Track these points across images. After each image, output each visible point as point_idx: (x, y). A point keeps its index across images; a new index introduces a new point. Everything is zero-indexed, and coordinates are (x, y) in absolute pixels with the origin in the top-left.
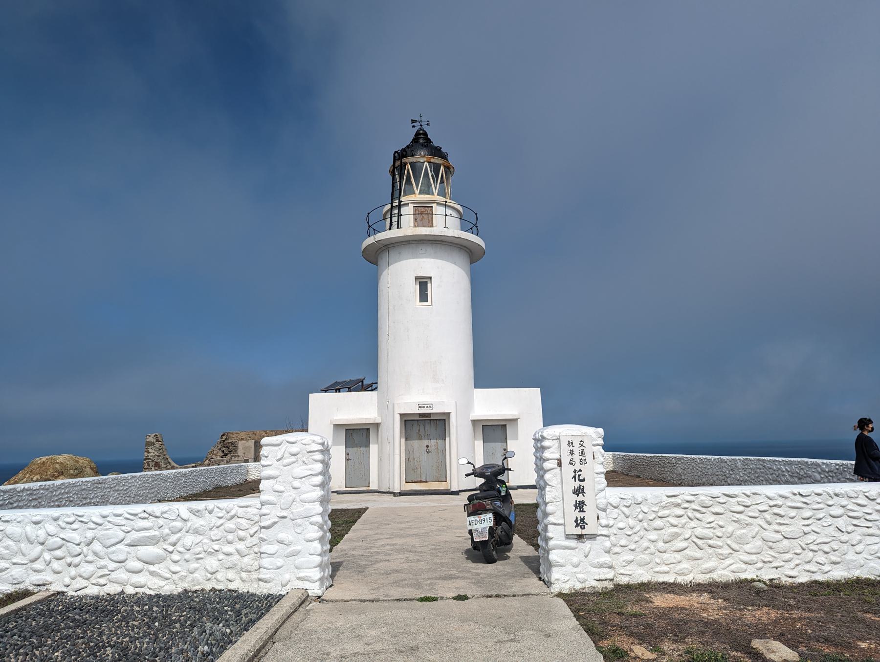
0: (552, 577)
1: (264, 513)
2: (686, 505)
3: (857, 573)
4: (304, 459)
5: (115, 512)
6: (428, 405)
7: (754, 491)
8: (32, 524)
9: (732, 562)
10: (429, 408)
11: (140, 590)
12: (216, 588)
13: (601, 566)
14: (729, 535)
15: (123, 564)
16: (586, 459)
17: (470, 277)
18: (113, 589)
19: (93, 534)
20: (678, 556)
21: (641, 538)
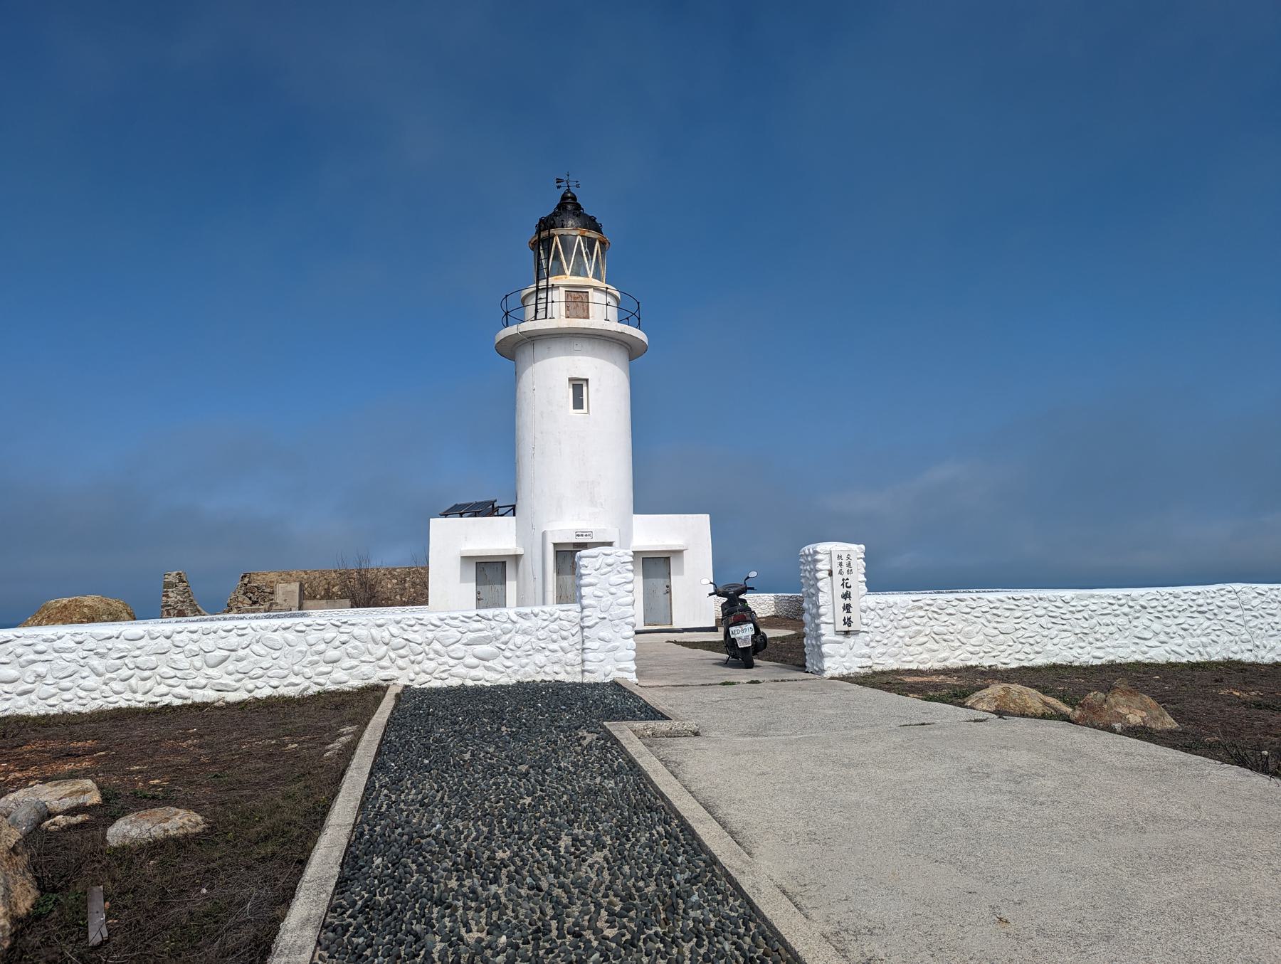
2: (927, 608)
3: (1054, 660)
4: (618, 569)
5: (452, 616)
7: (978, 596)
8: (376, 627)
9: (961, 652)
10: (588, 537)
13: (863, 656)
14: (959, 631)
15: (461, 661)
17: (628, 375)
18: (455, 682)
20: (920, 649)
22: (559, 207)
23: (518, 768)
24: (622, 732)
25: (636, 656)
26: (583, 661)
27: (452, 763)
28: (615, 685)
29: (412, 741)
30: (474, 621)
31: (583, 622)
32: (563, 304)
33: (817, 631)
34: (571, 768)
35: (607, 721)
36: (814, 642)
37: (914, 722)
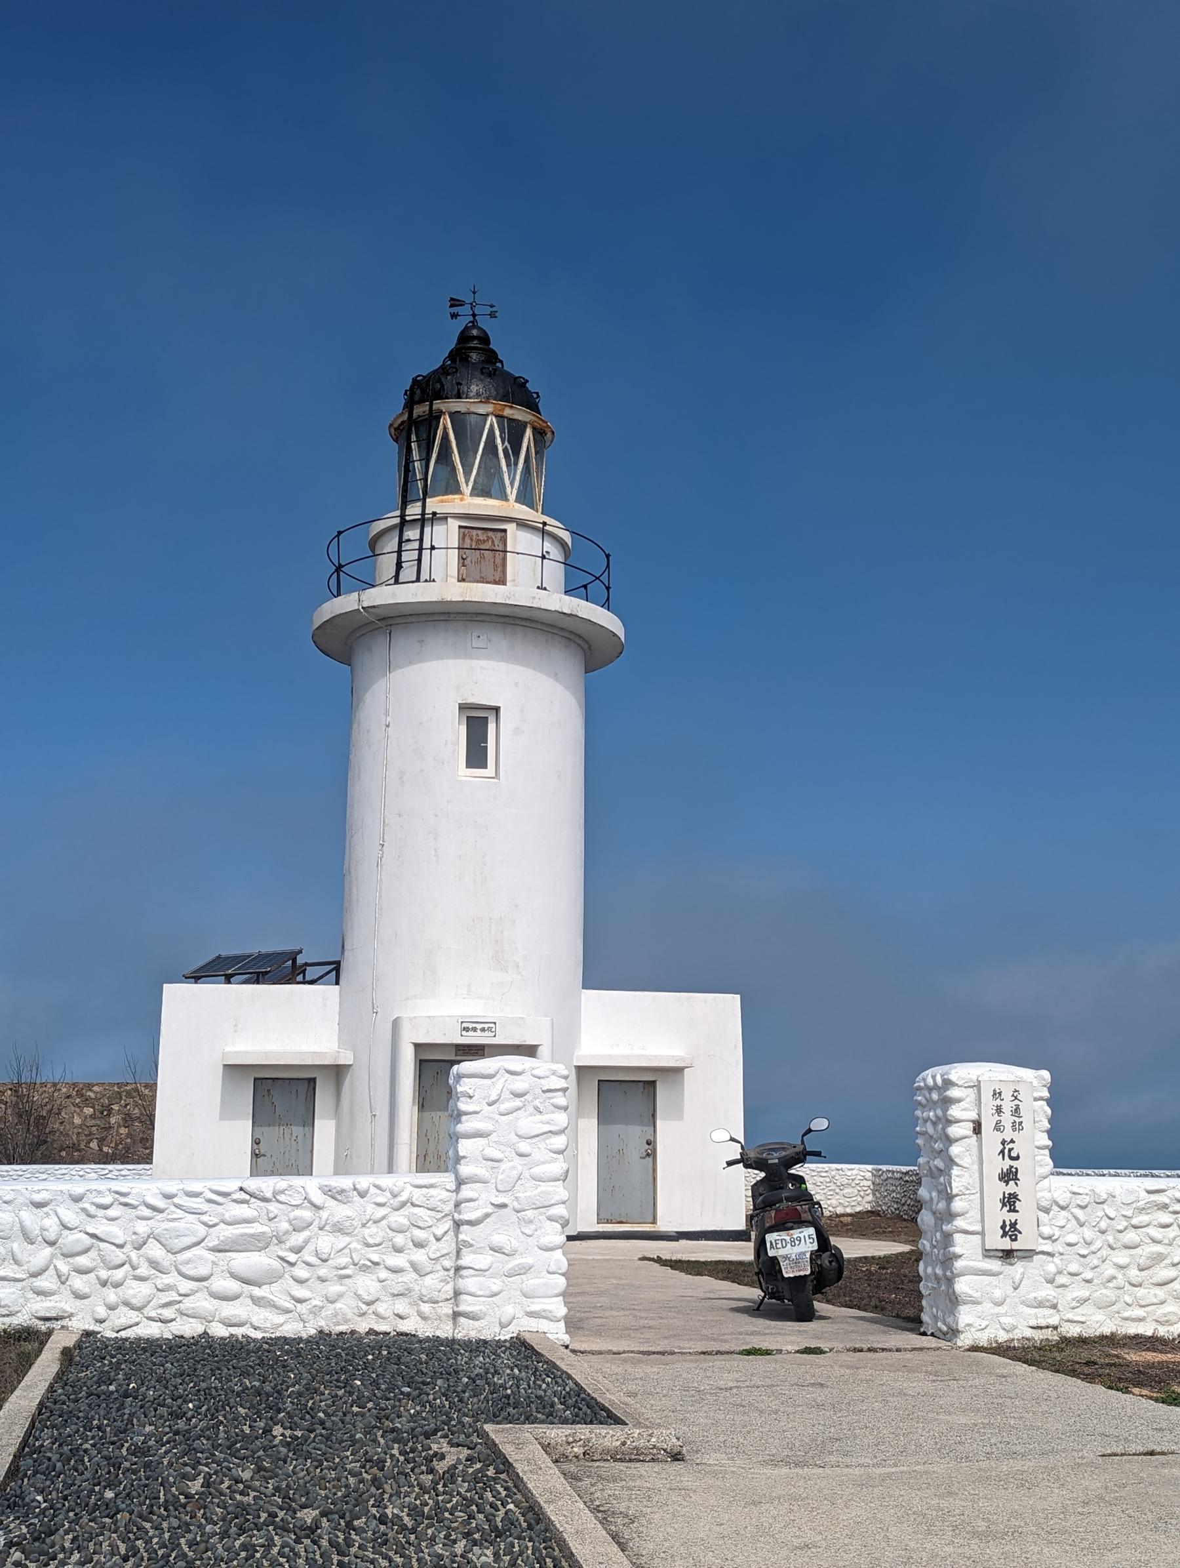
0: (960, 1321)
1: (468, 1197)
4: (537, 1103)
5: (189, 1189)
6: (486, 1026)
10: (486, 1033)
11: (238, 1332)
12: (376, 1329)
13: (1040, 1304)
15: (205, 1284)
16: (1022, 1122)
18: (189, 1328)
19: (148, 1227)
20: (1161, 1293)
21: (1103, 1262)
22: (453, 355)
23: (299, 1515)
24: (519, 1446)
25: (568, 1286)
26: (457, 1294)
27: (162, 1500)
28: (522, 1347)
29: (86, 1451)
30: (235, 1201)
31: (460, 1213)
32: (454, 555)
33: (945, 1248)
34: (406, 1519)
35: (494, 1422)
36: (939, 1271)
37: (1133, 1448)
